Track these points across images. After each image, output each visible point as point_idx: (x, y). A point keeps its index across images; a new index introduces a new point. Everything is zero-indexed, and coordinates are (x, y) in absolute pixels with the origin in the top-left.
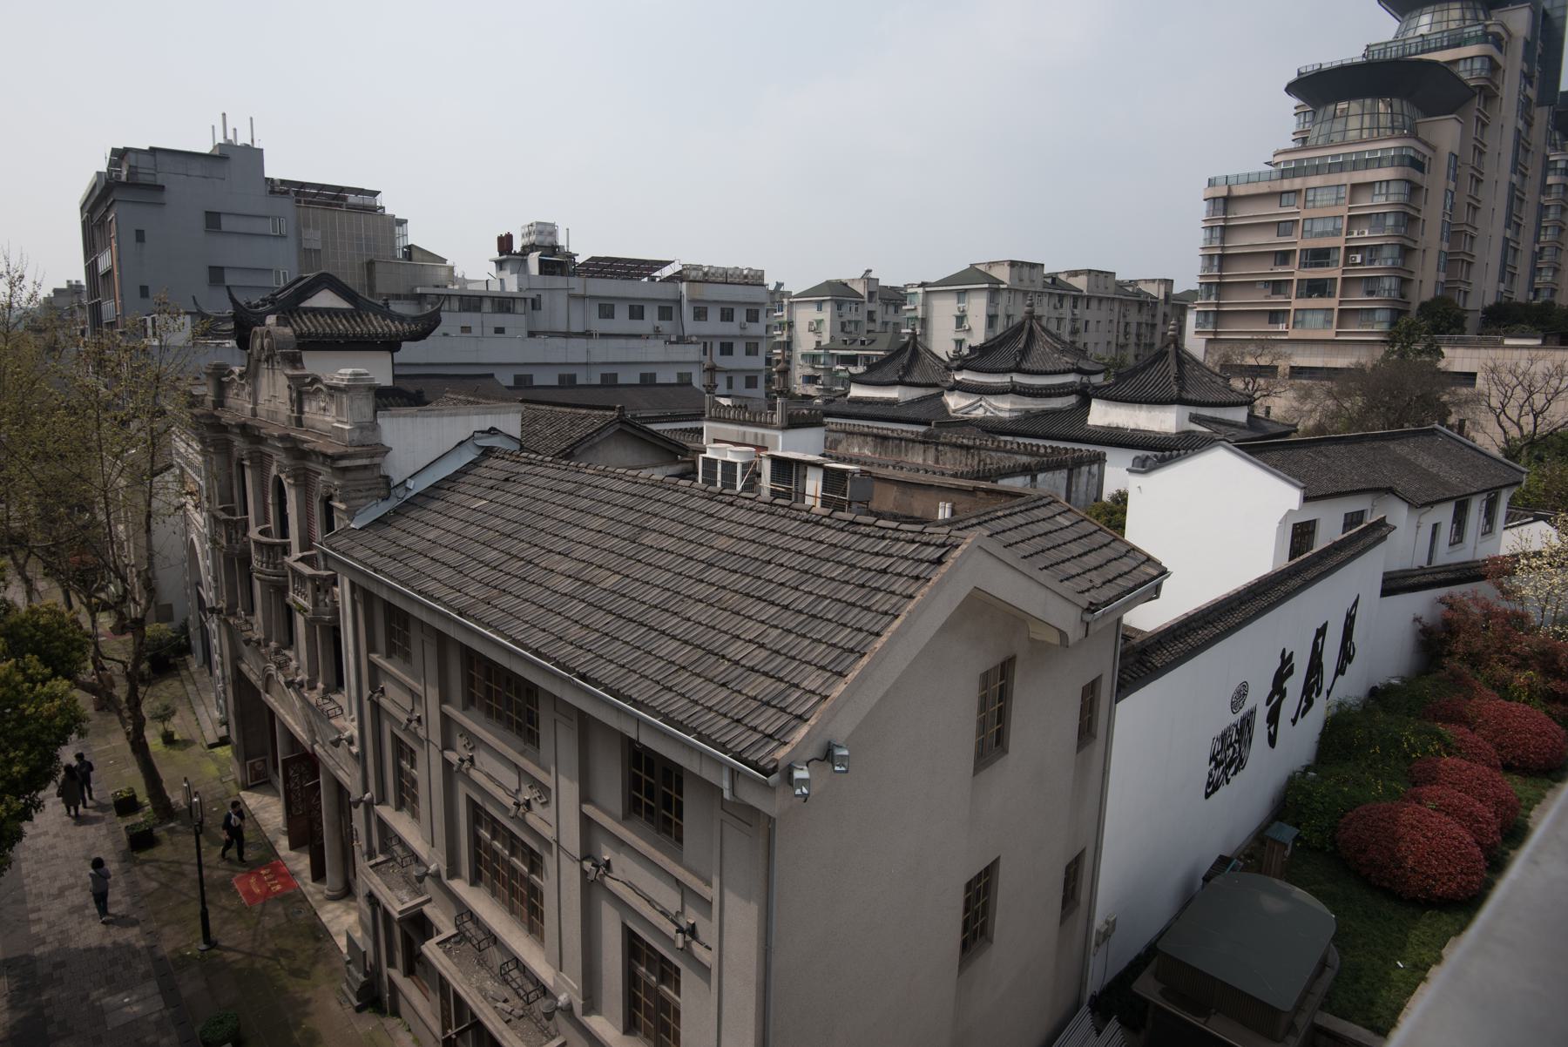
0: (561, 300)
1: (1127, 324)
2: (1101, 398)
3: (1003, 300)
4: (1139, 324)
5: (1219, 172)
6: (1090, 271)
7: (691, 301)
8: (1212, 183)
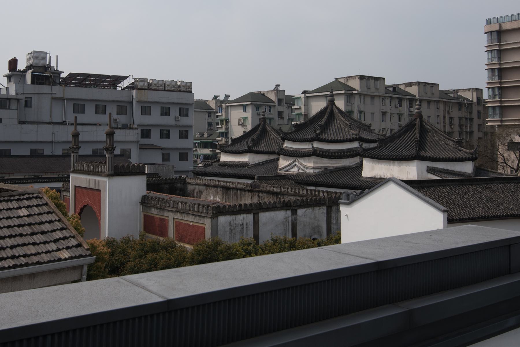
0: (46, 101)
1: (451, 118)
2: (366, 157)
3: (356, 101)
4: (460, 119)
5: (493, 15)
6: (404, 84)
7: (139, 102)
8: (489, 22)
